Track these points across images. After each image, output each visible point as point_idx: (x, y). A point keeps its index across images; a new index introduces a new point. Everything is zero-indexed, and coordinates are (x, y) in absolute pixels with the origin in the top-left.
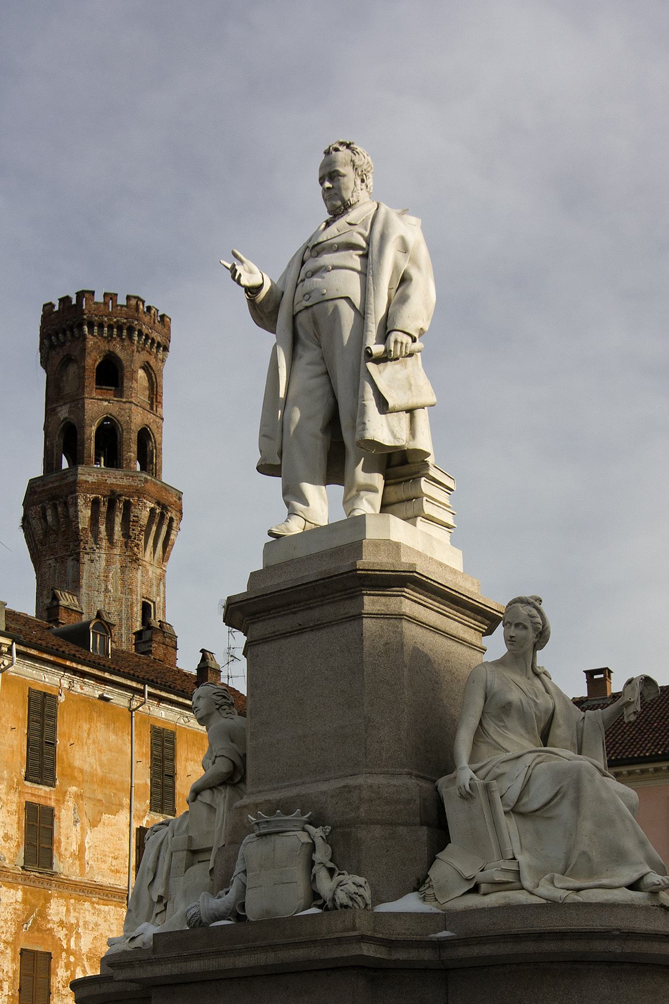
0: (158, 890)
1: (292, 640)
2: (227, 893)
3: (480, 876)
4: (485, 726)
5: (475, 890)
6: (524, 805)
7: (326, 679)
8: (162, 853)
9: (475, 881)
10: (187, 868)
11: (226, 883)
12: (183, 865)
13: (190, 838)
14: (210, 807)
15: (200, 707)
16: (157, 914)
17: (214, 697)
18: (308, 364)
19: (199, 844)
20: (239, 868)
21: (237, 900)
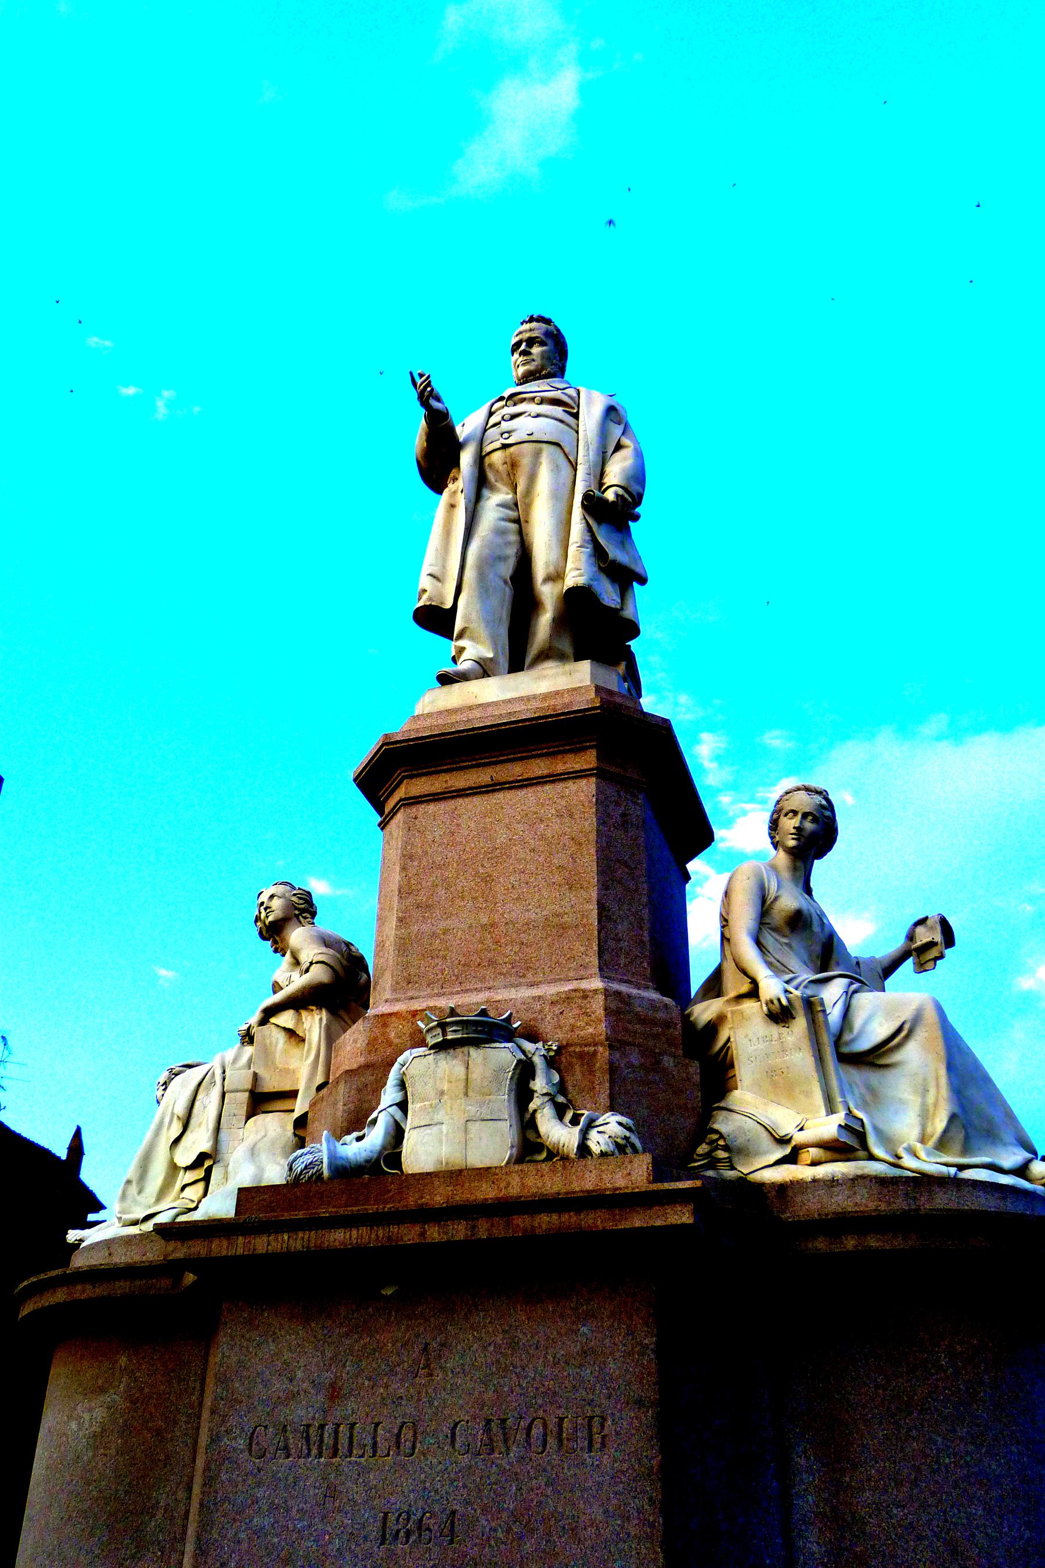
0: (198, 1141)
1: (477, 800)
2: (359, 1139)
3: (799, 1138)
4: (763, 941)
5: (791, 1159)
6: (848, 1044)
7: (533, 850)
8: (199, 1097)
9: (793, 1143)
10: (248, 1118)
11: (357, 1121)
12: (243, 1111)
13: (255, 1076)
14: (291, 1033)
15: (274, 908)
16: (183, 1188)
17: (294, 899)
18: (498, 505)
19: (272, 1083)
20: (389, 1095)
21: (384, 1148)
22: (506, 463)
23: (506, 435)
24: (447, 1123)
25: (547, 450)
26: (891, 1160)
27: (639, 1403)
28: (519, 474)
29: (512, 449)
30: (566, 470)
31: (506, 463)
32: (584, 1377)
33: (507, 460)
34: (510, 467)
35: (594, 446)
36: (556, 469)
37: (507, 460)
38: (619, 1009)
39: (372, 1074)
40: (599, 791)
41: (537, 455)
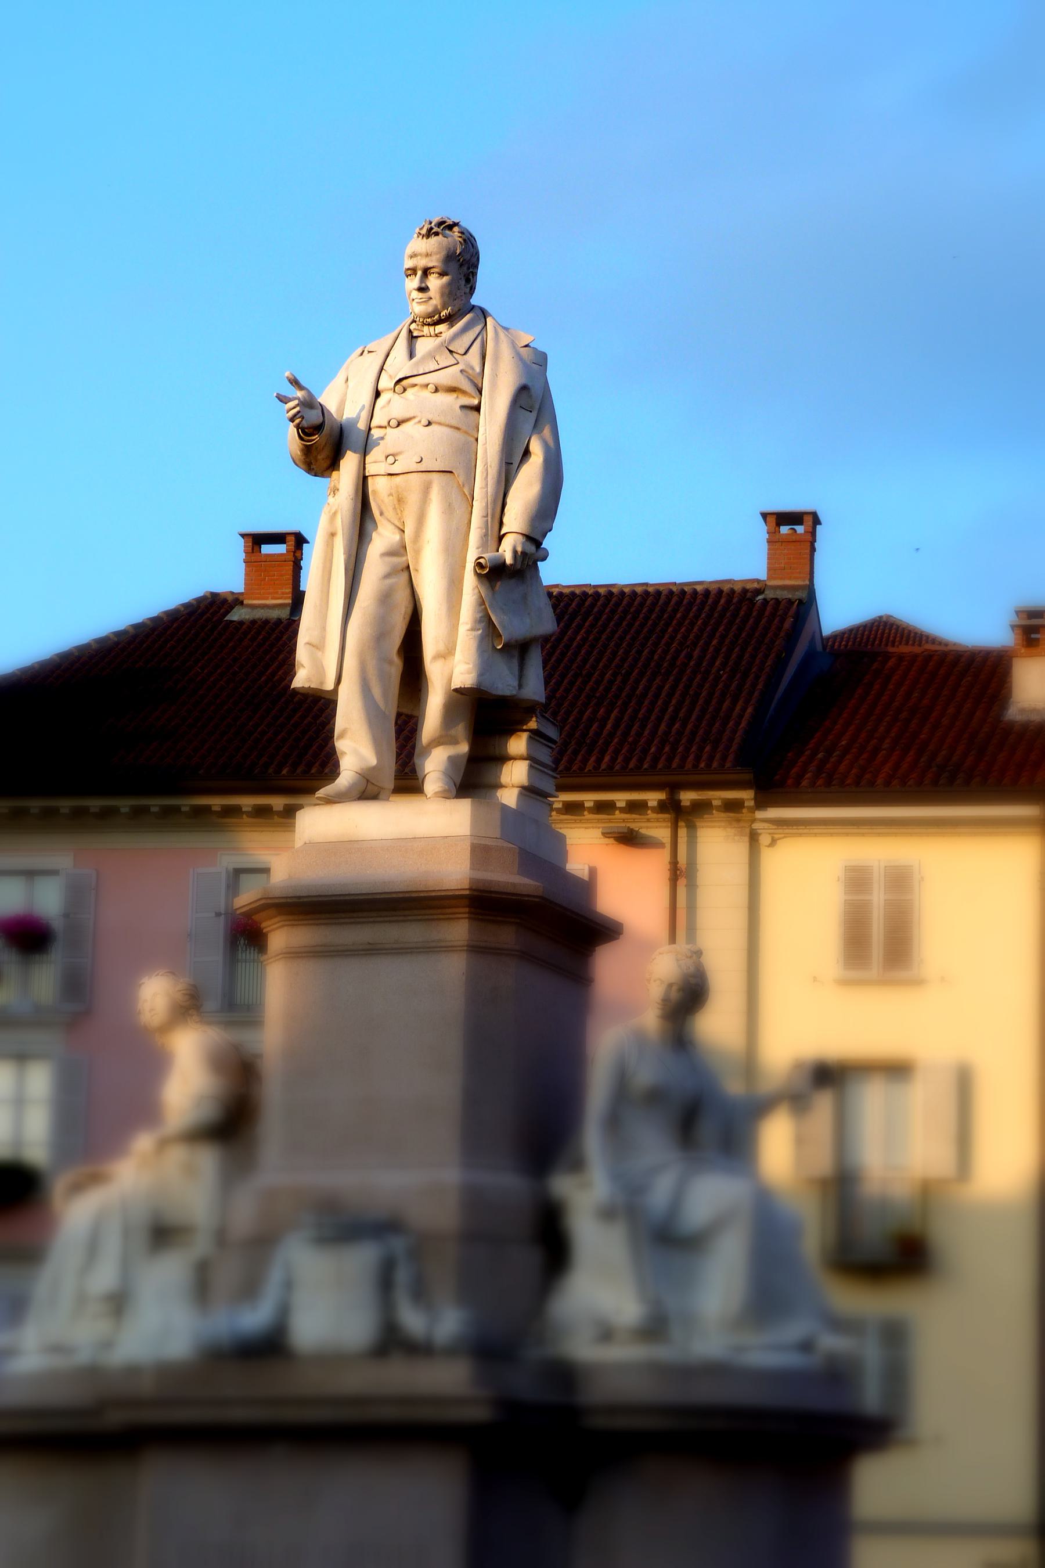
11: (249, 1289)
22: (391, 494)
23: (391, 459)
24: (325, 1306)
25: (437, 480)
26: (398, 524)
27: (379, 534)
28: (406, 513)
29: (398, 479)
30: (460, 511)
31: (391, 494)
32: (422, 1507)
33: (393, 491)
34: (396, 502)
35: (493, 472)
36: (449, 509)
37: (393, 491)
38: (474, 1201)
39: (261, 1244)
40: (480, 1002)
41: (426, 489)
